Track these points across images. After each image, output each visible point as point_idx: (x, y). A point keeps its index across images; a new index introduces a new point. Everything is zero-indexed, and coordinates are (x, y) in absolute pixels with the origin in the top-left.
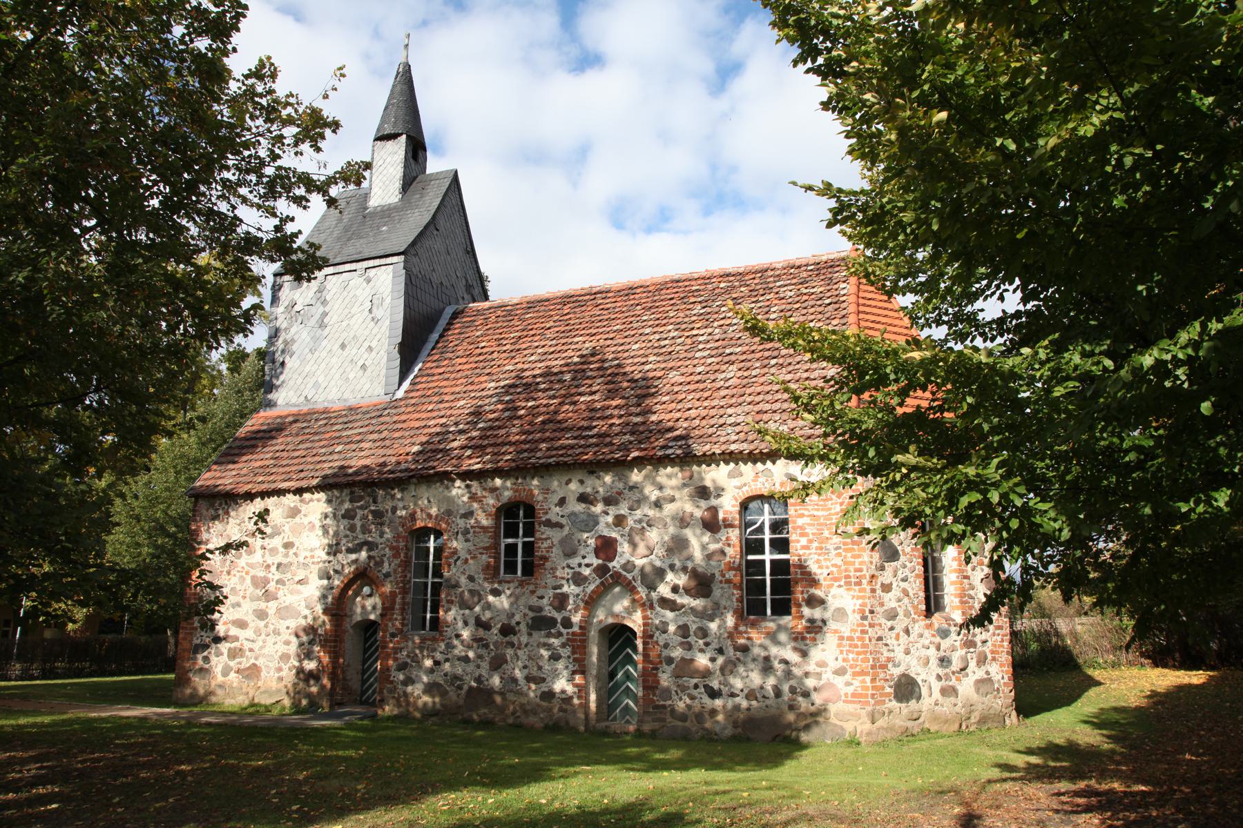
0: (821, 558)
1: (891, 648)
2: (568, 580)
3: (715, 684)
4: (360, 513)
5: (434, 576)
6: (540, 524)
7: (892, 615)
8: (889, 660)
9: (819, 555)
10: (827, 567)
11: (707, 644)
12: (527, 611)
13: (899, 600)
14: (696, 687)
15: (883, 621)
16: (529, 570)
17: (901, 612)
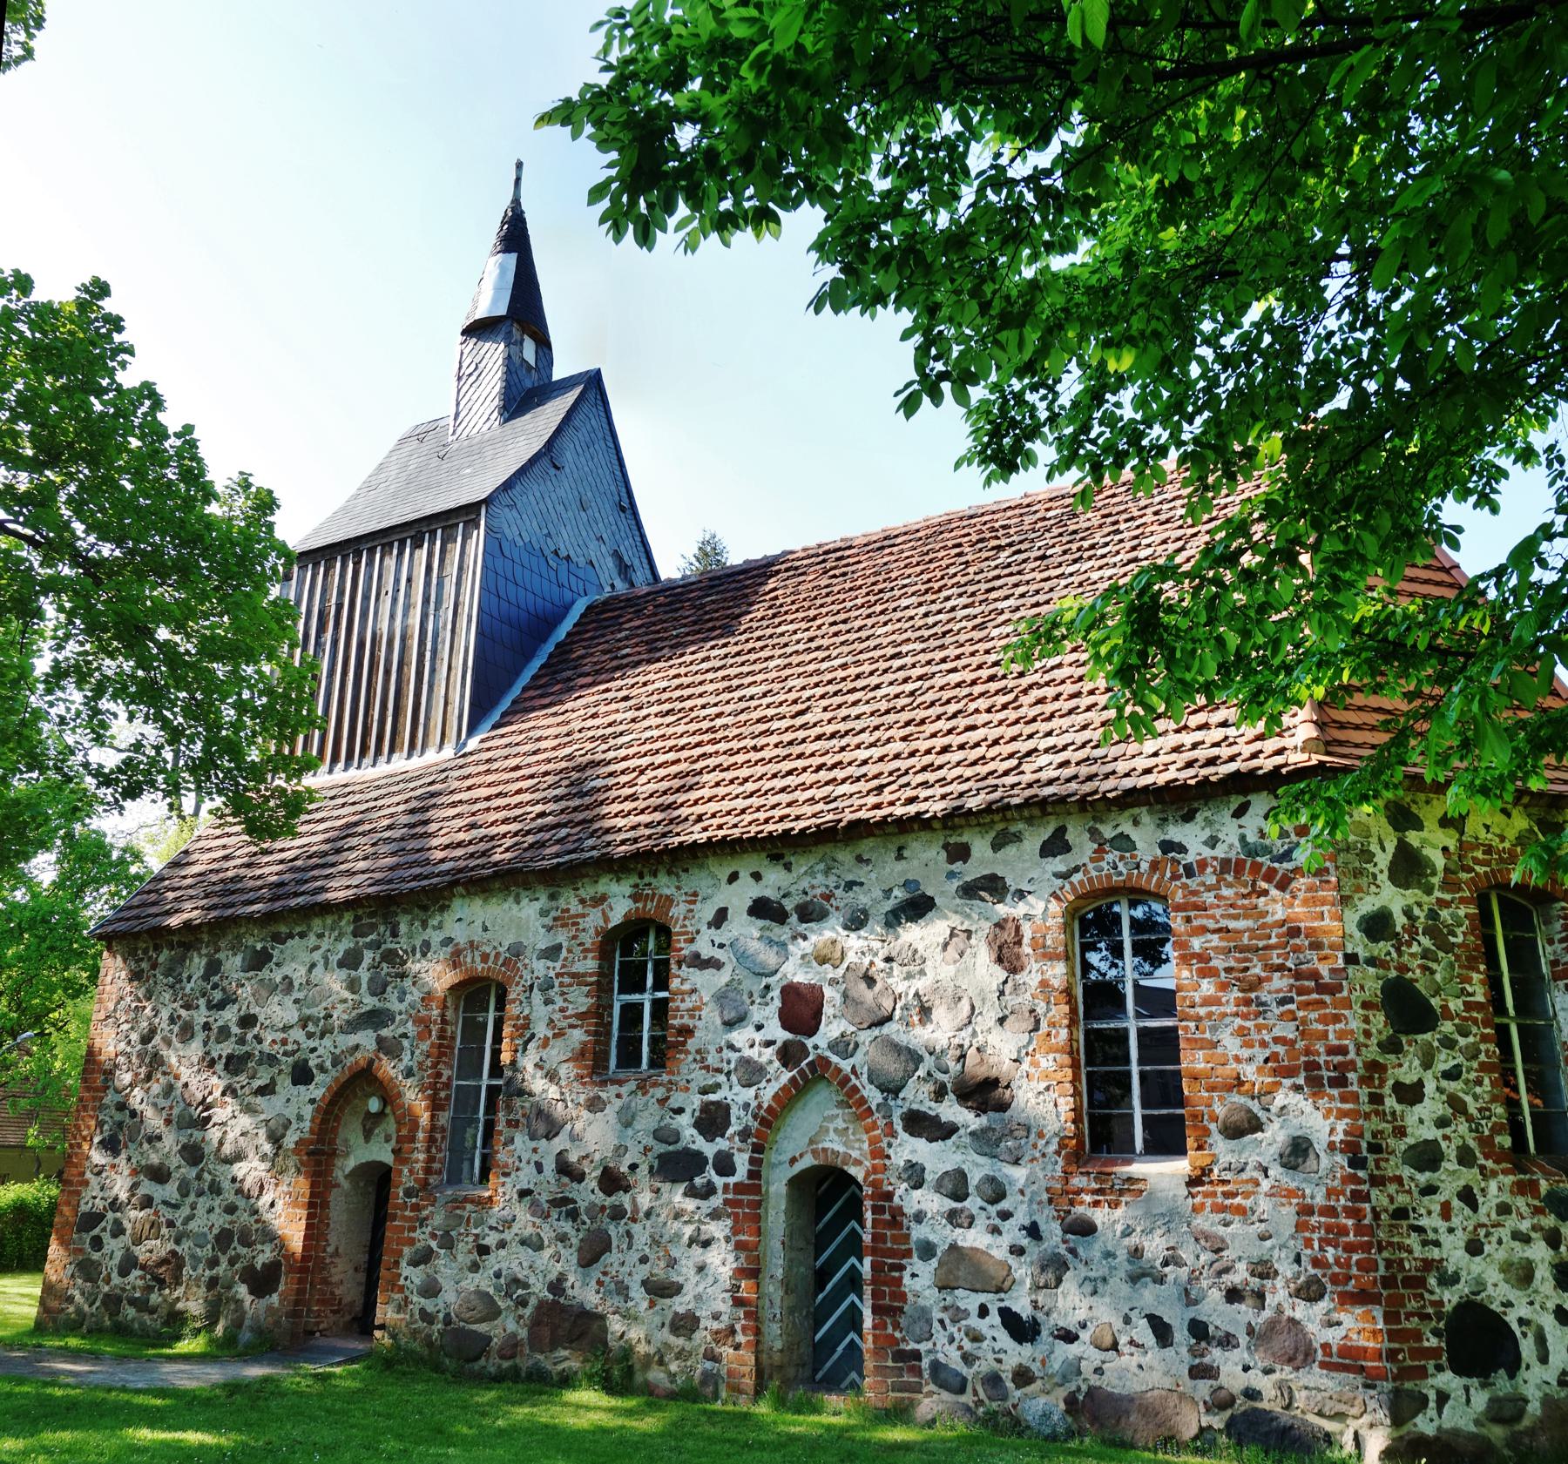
0: (1249, 1024)
1: (1432, 1236)
2: (728, 1074)
3: (1021, 1304)
4: (368, 956)
5: (492, 1075)
6: (679, 964)
7: (1428, 1156)
8: (1428, 1265)
9: (1245, 1017)
10: (1264, 1044)
11: (1005, 1215)
12: (650, 1141)
13: (1442, 1123)
14: (983, 1312)
15: (1406, 1172)
16: (658, 1061)
17: (1449, 1149)
